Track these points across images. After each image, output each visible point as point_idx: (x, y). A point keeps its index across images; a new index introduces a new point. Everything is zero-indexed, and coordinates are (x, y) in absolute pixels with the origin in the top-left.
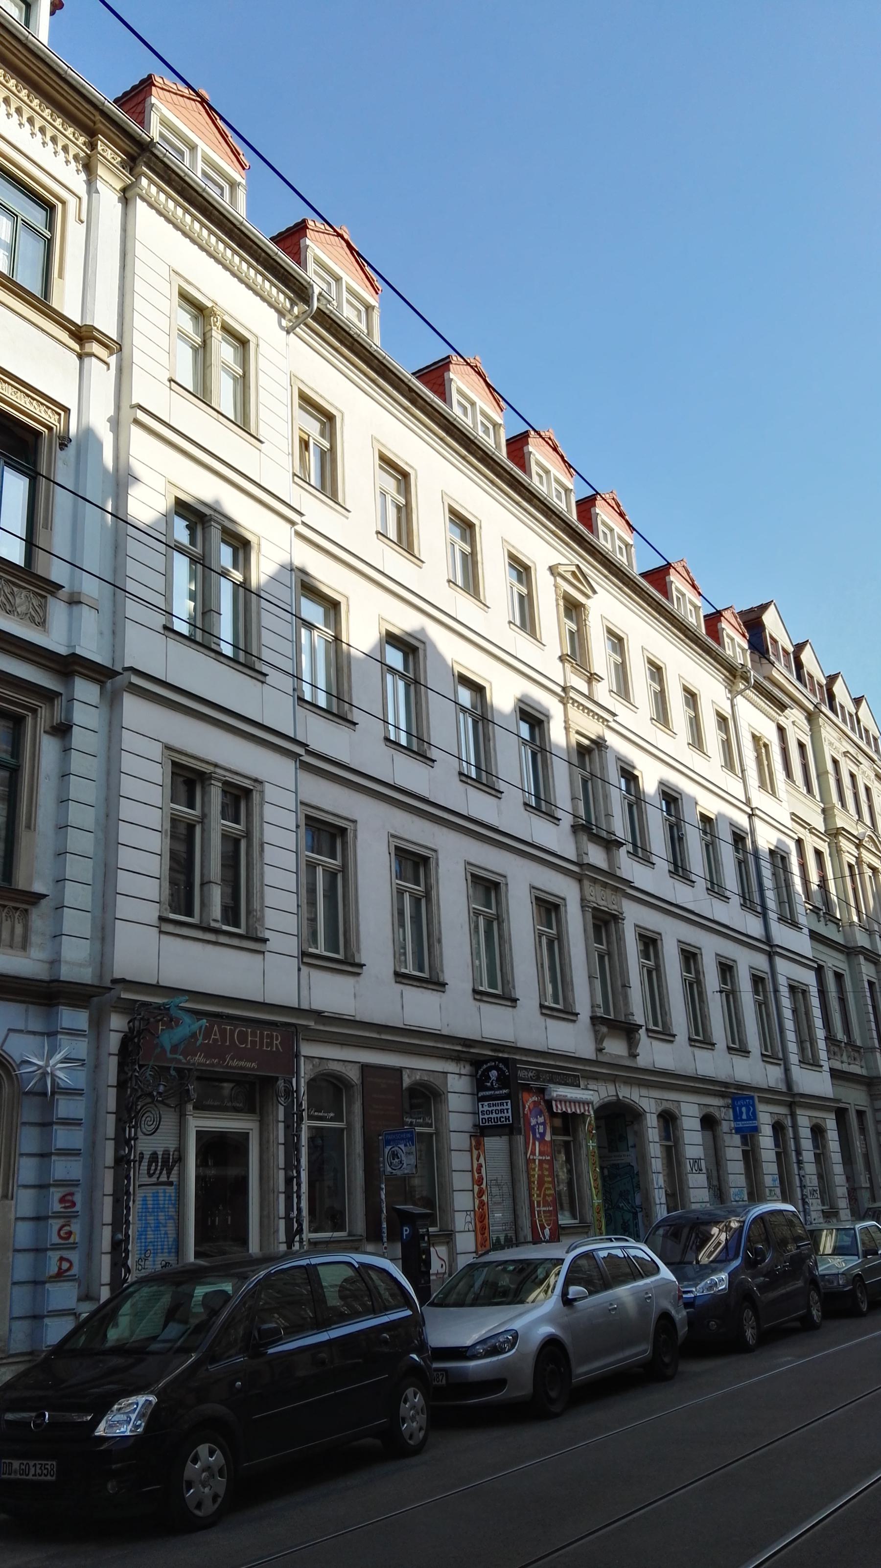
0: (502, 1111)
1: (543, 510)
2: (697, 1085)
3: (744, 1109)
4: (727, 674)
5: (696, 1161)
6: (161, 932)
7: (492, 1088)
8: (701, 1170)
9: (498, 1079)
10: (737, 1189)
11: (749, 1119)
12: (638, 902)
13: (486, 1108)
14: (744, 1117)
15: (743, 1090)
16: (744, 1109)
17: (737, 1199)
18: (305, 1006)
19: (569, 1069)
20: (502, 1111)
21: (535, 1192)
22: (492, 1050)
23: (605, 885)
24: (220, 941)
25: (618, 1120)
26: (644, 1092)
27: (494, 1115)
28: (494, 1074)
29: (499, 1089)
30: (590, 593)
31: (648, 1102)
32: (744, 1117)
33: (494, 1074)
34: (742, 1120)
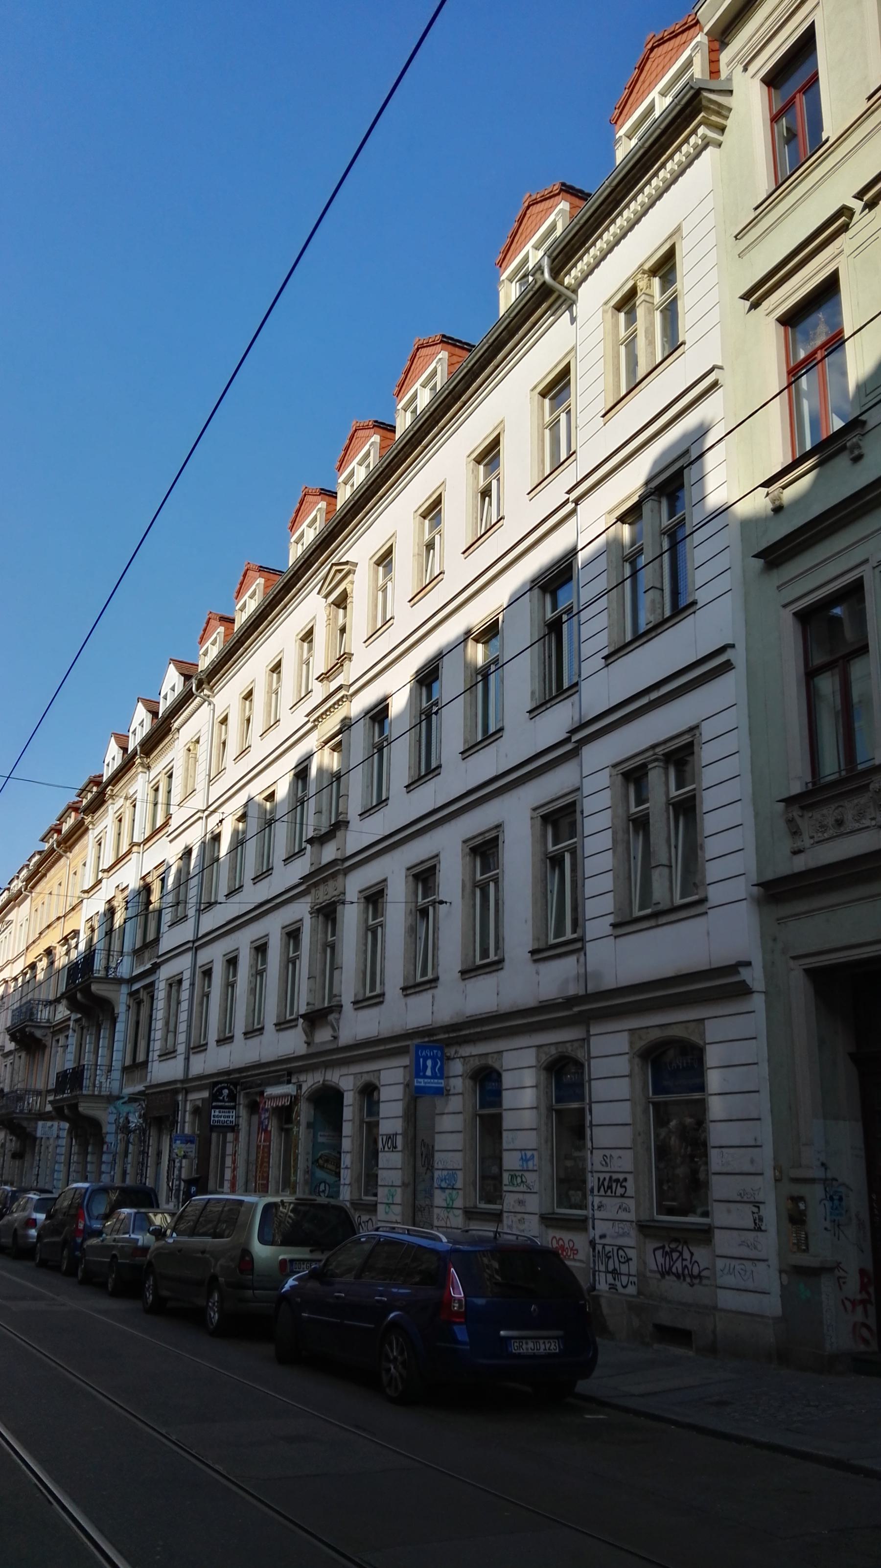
0: (229, 1117)
1: (677, 128)
2: (388, 1047)
3: (429, 1063)
4: (544, 306)
5: (391, 1137)
6: (616, 937)
7: (223, 1101)
8: (395, 1147)
9: (228, 1096)
10: (445, 1173)
11: (434, 1076)
12: (394, 848)
13: (217, 1114)
14: (429, 1073)
15: (460, 1030)
16: (429, 1063)
17: (443, 1185)
18: (591, 989)
19: (284, 1069)
20: (229, 1117)
21: (259, 1169)
22: (444, 1033)
23: (325, 880)
24: (660, 923)
25: (328, 1101)
26: (344, 1070)
27: (222, 1119)
28: (226, 1092)
29: (228, 1102)
30: (324, 592)
31: (346, 1081)
32: (429, 1073)
33: (226, 1092)
34: (425, 1077)
